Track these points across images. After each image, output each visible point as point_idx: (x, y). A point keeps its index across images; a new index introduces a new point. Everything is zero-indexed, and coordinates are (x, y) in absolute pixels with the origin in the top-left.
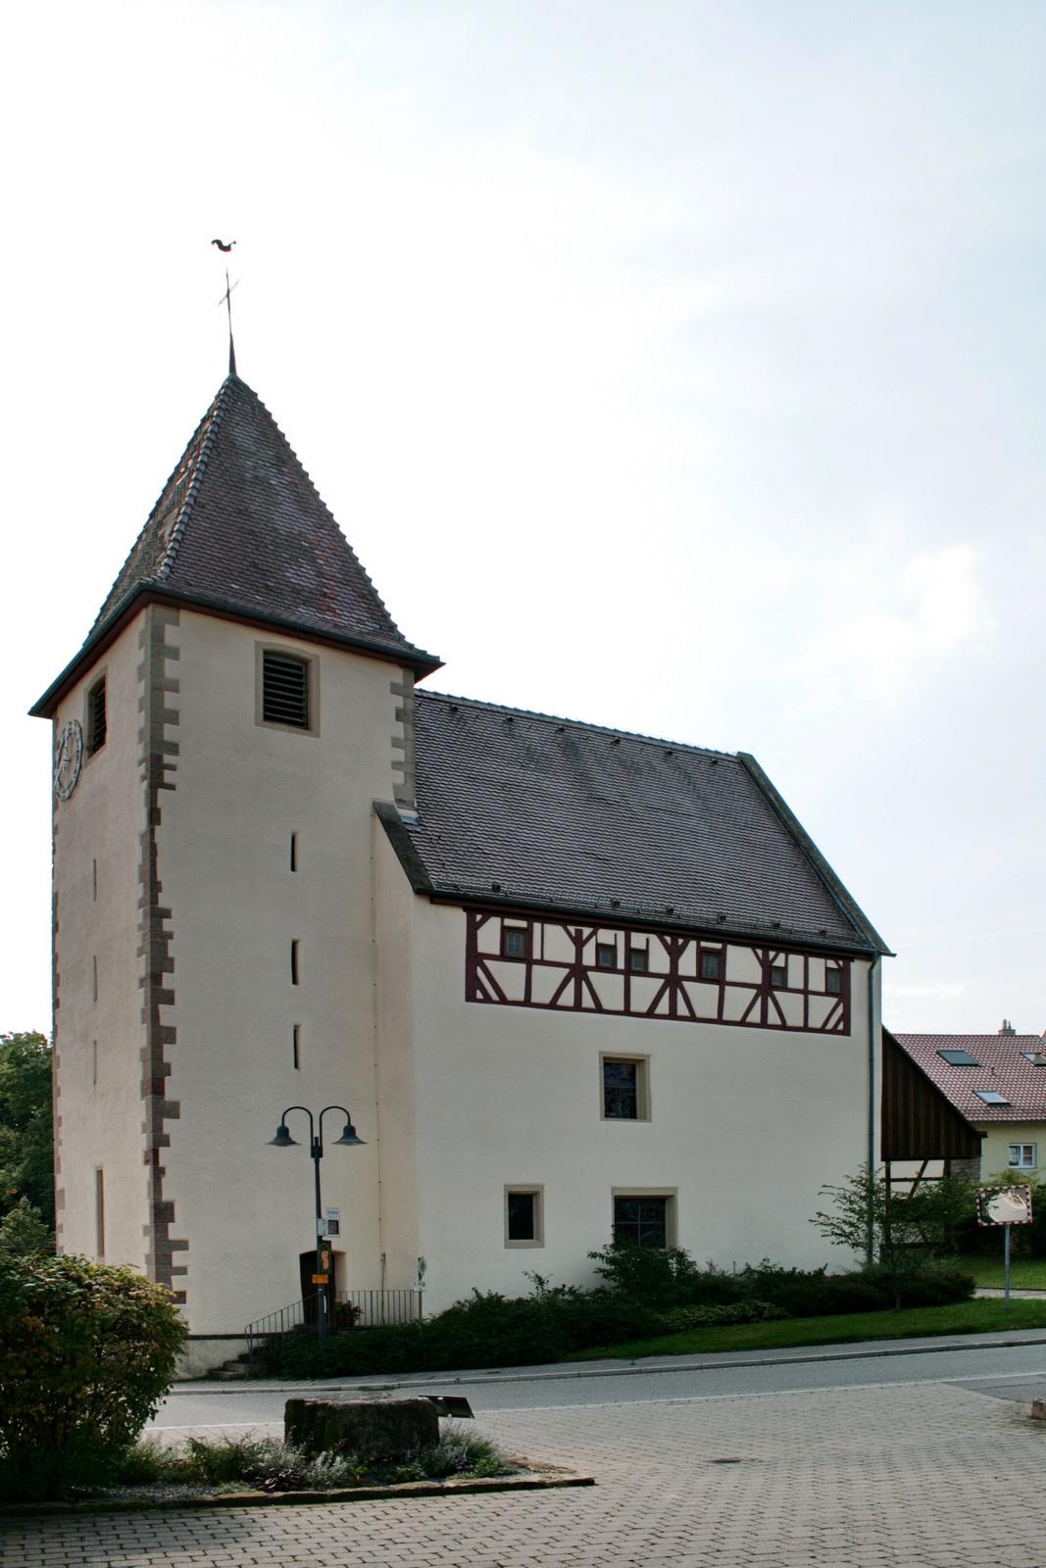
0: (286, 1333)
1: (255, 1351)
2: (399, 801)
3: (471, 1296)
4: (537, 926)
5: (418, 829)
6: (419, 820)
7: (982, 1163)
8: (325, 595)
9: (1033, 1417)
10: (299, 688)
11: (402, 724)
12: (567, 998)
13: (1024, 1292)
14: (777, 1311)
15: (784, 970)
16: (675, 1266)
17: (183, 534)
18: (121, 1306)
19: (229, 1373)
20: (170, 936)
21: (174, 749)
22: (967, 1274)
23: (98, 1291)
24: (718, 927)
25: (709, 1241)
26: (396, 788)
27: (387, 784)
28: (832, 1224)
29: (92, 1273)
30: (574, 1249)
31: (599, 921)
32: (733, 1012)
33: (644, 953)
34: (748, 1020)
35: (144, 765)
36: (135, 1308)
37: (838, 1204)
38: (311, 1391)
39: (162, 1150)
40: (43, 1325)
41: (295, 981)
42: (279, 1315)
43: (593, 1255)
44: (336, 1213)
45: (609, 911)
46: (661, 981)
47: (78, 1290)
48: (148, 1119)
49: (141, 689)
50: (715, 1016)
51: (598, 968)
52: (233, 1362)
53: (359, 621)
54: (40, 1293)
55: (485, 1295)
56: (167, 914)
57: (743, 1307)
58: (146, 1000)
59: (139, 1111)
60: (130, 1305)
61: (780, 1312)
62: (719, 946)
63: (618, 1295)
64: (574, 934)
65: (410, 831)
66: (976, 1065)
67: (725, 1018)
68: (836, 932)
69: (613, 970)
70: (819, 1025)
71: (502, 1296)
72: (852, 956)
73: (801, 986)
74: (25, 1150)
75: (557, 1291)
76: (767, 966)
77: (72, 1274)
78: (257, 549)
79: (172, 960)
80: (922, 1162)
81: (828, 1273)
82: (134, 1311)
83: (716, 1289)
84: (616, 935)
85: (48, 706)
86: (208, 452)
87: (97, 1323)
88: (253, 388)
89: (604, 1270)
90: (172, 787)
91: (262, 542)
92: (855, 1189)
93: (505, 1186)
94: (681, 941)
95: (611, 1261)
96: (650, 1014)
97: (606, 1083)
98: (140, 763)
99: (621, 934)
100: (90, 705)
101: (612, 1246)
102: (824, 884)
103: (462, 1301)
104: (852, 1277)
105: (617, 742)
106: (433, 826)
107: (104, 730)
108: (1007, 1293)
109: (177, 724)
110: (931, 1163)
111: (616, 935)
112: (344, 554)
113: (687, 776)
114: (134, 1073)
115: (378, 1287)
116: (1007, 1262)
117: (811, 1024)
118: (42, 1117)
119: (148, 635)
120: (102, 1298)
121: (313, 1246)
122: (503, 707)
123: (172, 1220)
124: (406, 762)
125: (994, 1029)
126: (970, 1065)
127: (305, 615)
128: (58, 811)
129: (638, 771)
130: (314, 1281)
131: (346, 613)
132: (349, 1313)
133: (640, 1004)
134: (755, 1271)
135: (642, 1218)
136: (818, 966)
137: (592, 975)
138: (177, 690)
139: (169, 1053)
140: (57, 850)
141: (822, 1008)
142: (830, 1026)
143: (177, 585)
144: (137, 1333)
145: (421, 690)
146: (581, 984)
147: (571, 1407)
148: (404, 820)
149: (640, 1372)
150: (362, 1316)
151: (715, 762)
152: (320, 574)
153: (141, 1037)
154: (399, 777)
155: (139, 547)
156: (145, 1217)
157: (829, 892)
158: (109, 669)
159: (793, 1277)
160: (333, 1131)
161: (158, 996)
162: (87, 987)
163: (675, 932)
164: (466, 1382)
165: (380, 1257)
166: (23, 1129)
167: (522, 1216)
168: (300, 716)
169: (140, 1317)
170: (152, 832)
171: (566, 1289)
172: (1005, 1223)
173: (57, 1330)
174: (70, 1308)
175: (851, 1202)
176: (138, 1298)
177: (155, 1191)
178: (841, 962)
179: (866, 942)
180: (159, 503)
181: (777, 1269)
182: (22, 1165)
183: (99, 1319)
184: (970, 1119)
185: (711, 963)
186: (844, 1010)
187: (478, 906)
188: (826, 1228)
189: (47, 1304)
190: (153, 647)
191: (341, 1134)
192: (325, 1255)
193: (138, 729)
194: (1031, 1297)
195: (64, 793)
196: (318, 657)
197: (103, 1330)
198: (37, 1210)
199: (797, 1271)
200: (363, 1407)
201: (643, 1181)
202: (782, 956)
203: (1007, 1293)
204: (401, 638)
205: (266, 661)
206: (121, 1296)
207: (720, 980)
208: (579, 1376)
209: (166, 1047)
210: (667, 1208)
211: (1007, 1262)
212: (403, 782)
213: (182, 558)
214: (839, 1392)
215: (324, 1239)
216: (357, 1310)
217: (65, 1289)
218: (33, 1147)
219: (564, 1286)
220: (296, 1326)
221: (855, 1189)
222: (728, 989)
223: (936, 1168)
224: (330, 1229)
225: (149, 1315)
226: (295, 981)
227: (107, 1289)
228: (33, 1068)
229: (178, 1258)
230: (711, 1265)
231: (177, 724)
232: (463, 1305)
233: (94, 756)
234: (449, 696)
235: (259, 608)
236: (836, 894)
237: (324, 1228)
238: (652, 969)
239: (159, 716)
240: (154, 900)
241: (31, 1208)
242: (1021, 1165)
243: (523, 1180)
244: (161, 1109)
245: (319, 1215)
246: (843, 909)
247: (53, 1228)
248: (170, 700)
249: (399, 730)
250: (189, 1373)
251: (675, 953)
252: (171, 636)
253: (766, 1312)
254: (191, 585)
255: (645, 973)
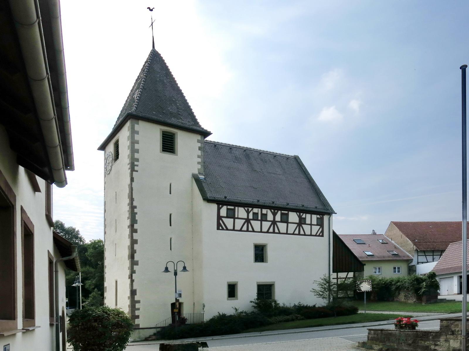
0: (166, 327)
1: (158, 332)
2: (199, 173)
3: (217, 314)
4: (237, 208)
5: (205, 181)
6: (205, 178)
7: (364, 273)
8: (179, 114)
9: (358, 346)
10: (172, 142)
11: (200, 151)
12: (245, 228)
13: (373, 311)
14: (302, 317)
15: (305, 219)
16: (274, 305)
17: (138, 103)
18: (117, 319)
19: (151, 339)
20: (136, 213)
21: (137, 160)
22: (356, 306)
23: (111, 315)
24: (287, 207)
25: (284, 297)
26: (199, 169)
27: (196, 168)
28: (317, 292)
29: (110, 311)
30: (246, 299)
31: (253, 206)
32: (291, 231)
33: (266, 215)
34: (295, 233)
35: (129, 165)
36: (120, 319)
37: (318, 286)
38: (166, 342)
39: (133, 275)
40: (97, 325)
41: (170, 225)
42: (165, 321)
43: (251, 302)
44: (181, 291)
45: (257, 203)
46: (271, 223)
47: (106, 315)
48: (130, 266)
49: (128, 143)
50: (285, 232)
51: (253, 219)
52: (152, 335)
53: (189, 122)
54: (96, 317)
55: (221, 314)
56: (135, 207)
57: (292, 316)
58: (130, 232)
59: (127, 263)
60: (119, 319)
61: (304, 317)
62: (287, 212)
63: (258, 313)
64: (247, 210)
65: (202, 182)
66: (364, 244)
67: (288, 233)
68: (320, 208)
69: (257, 220)
70: (315, 234)
71: (226, 314)
72: (324, 214)
73: (310, 223)
74: (96, 275)
75: (241, 312)
76: (300, 217)
77: (107, 311)
78: (160, 101)
79: (137, 220)
80: (347, 273)
81: (317, 306)
82: (120, 320)
83: (285, 311)
84: (116, 305)
85: (103, 147)
86: (147, 73)
87: (111, 324)
88: (159, 52)
89: (254, 306)
90: (137, 171)
91: (162, 99)
92: (323, 282)
93: (227, 282)
94: (276, 211)
95: (256, 303)
96: (268, 232)
97: (255, 252)
98: (128, 164)
99: (260, 210)
100: (115, 147)
101: (256, 299)
102: (317, 193)
103: (215, 316)
104: (323, 307)
105: (260, 153)
106: (208, 179)
107: (119, 154)
108: (365, 312)
109: (138, 153)
110: (350, 273)
111: (116, 305)
112: (184, 102)
113: (280, 163)
114: (126, 253)
115: (192, 313)
116: (365, 302)
117: (313, 234)
118: (102, 264)
119: (130, 128)
120: (112, 317)
121: (174, 301)
122: (229, 145)
123: (136, 295)
124: (201, 162)
125: (370, 232)
126: (363, 244)
127: (173, 121)
128: (106, 178)
129: (266, 162)
130: (174, 311)
131: (185, 120)
132: (183, 320)
133: (265, 229)
134: (297, 306)
135: (265, 291)
136: (315, 217)
137: (251, 221)
138: (138, 143)
139: (136, 247)
140: (105, 189)
141: (316, 229)
142: (318, 234)
143: (138, 113)
144: (121, 326)
145: (206, 140)
146: (248, 224)
147: (240, 345)
148: (201, 179)
149: (262, 336)
150: (188, 321)
151: (288, 158)
152: (178, 108)
153: (128, 242)
154: (199, 166)
155: (129, 97)
156: (128, 294)
157: (318, 195)
158: (120, 137)
159: (307, 307)
160: (180, 268)
161: (133, 230)
162: (113, 229)
163: (274, 209)
164: (214, 340)
165: (193, 304)
166: (96, 268)
167: (232, 291)
168: (172, 150)
169: (122, 322)
170: (131, 184)
171: (244, 312)
172: (364, 291)
173: (100, 326)
174: (104, 320)
175: (322, 286)
176: (121, 317)
177: (131, 287)
178: (321, 216)
179: (328, 210)
180: (133, 87)
181: (303, 305)
182: (96, 279)
183: (111, 323)
184: (361, 260)
185: (285, 217)
186: (322, 229)
187: (220, 203)
188: (315, 293)
189: (98, 319)
190: (132, 131)
191: (182, 269)
192: (177, 304)
193: (128, 155)
194: (373, 313)
195: (108, 172)
196: (177, 132)
197: (112, 326)
198: (99, 292)
199: (308, 306)
200: (179, 345)
201: (265, 279)
202: (304, 215)
203: (365, 312)
204: (200, 126)
205: (163, 134)
206: (117, 317)
207: (287, 222)
208: (245, 337)
209: (135, 245)
210: (272, 288)
211: (365, 302)
212: (200, 168)
213: (139, 105)
214: (311, 340)
215: (177, 299)
216: (186, 319)
217: (103, 315)
218: (99, 274)
219: (243, 311)
220: (169, 324)
221: (323, 282)
222: (289, 224)
223: (351, 275)
224: (179, 296)
225: (124, 321)
226: (170, 225)
227: (113, 315)
228: (99, 250)
229: (137, 306)
230: (284, 304)
231: (138, 153)
232: (215, 317)
233: (116, 162)
234: (214, 142)
235: (161, 119)
236: (320, 196)
237: (177, 296)
238: (268, 219)
239: (134, 151)
240: (132, 203)
241: (98, 292)
242: (377, 273)
243: (232, 280)
244: (133, 262)
245: (176, 292)
246: (322, 200)
247: (103, 298)
248: (137, 146)
249: (199, 153)
250: (140, 339)
251: (274, 215)
252: (137, 128)
253: (299, 318)
254: (142, 113)
255: (266, 221)
